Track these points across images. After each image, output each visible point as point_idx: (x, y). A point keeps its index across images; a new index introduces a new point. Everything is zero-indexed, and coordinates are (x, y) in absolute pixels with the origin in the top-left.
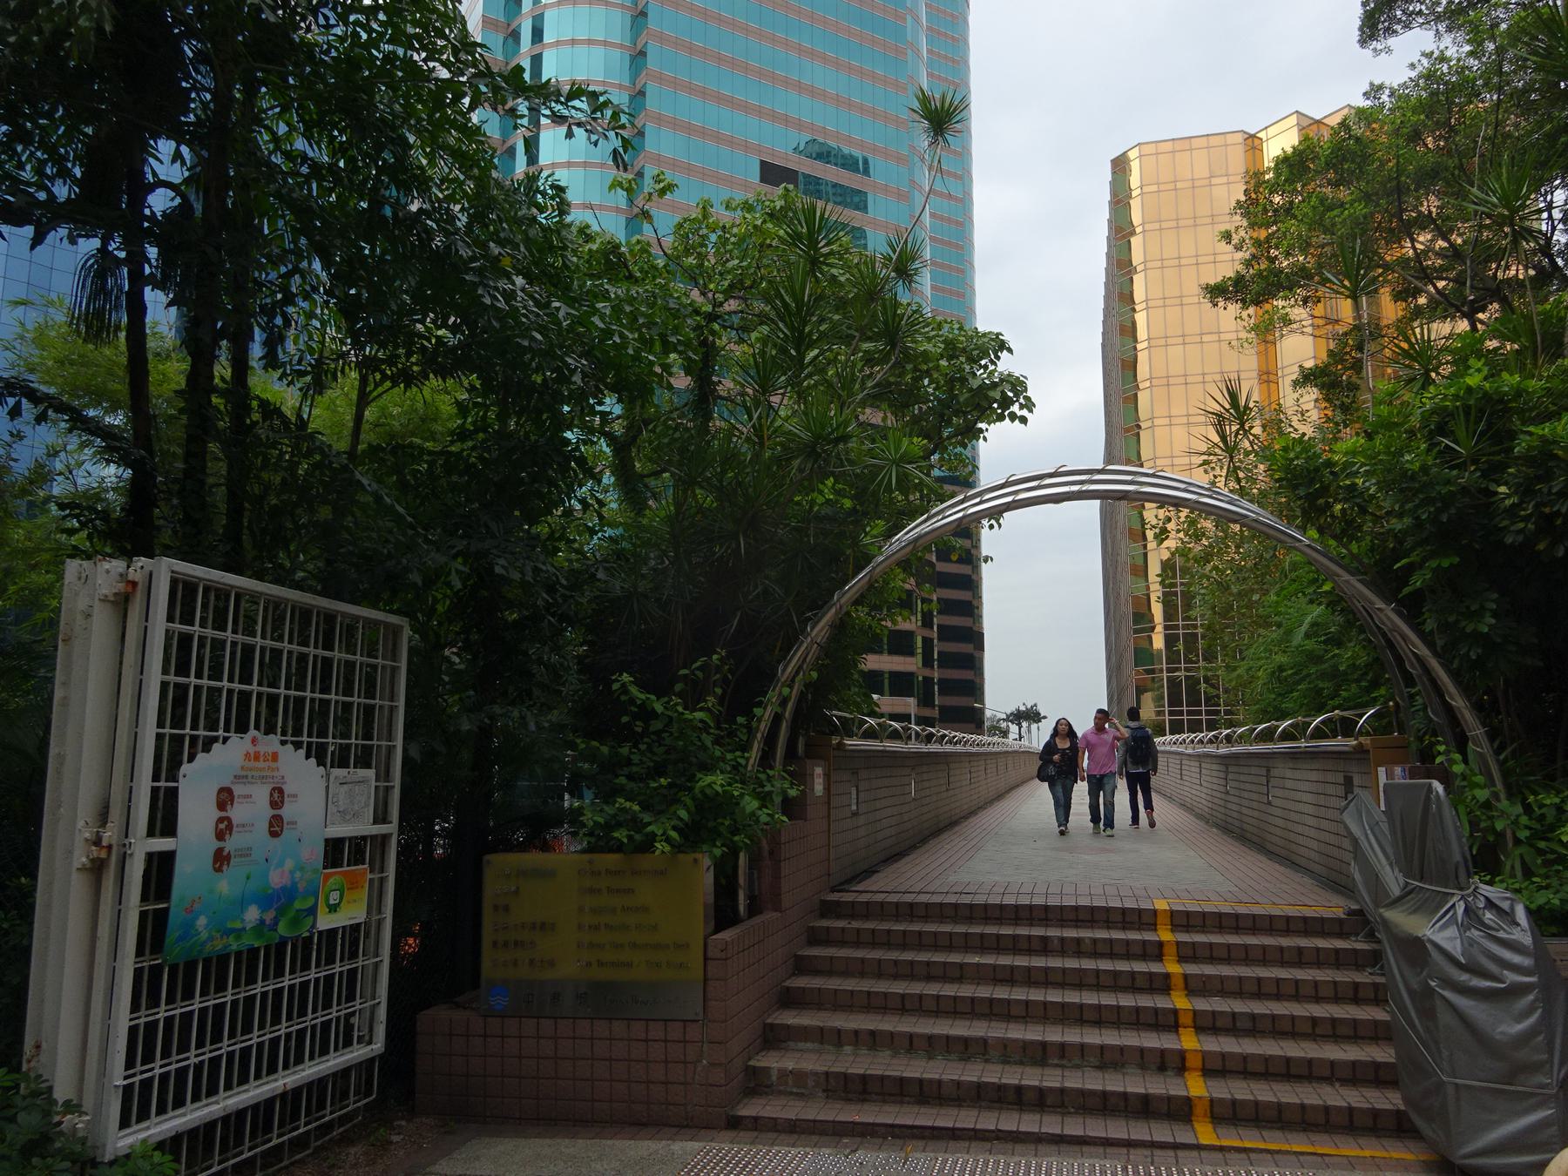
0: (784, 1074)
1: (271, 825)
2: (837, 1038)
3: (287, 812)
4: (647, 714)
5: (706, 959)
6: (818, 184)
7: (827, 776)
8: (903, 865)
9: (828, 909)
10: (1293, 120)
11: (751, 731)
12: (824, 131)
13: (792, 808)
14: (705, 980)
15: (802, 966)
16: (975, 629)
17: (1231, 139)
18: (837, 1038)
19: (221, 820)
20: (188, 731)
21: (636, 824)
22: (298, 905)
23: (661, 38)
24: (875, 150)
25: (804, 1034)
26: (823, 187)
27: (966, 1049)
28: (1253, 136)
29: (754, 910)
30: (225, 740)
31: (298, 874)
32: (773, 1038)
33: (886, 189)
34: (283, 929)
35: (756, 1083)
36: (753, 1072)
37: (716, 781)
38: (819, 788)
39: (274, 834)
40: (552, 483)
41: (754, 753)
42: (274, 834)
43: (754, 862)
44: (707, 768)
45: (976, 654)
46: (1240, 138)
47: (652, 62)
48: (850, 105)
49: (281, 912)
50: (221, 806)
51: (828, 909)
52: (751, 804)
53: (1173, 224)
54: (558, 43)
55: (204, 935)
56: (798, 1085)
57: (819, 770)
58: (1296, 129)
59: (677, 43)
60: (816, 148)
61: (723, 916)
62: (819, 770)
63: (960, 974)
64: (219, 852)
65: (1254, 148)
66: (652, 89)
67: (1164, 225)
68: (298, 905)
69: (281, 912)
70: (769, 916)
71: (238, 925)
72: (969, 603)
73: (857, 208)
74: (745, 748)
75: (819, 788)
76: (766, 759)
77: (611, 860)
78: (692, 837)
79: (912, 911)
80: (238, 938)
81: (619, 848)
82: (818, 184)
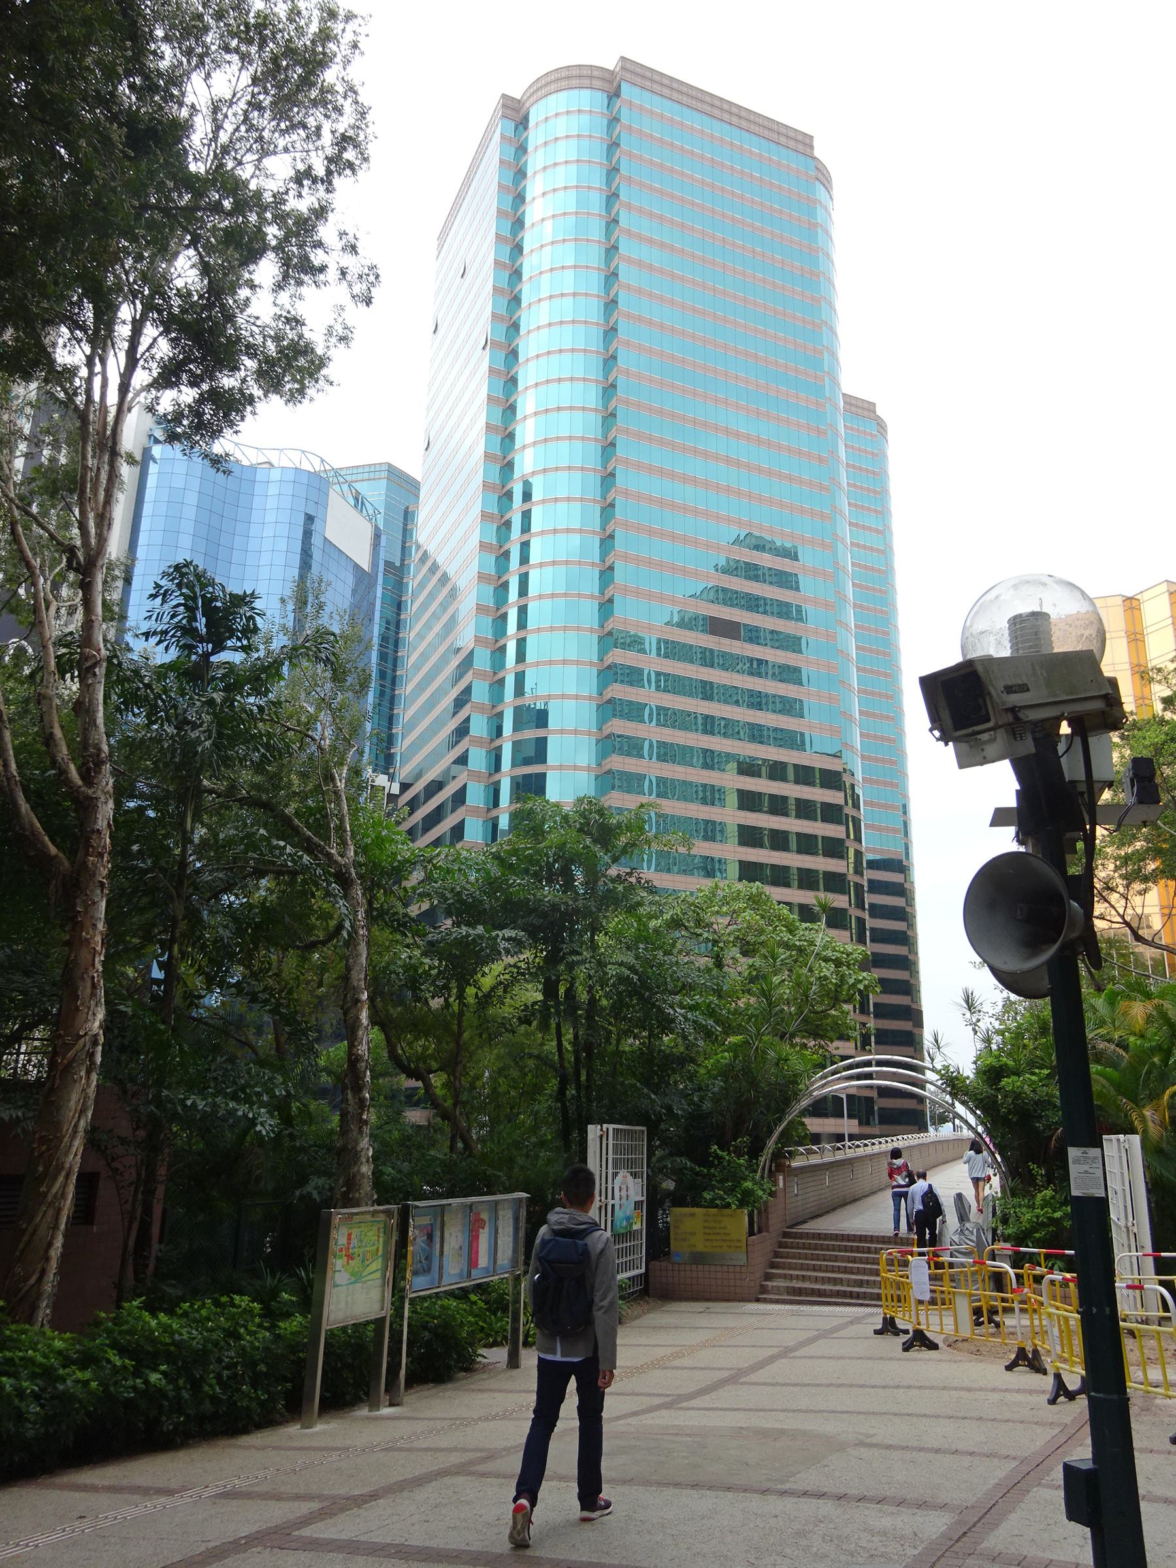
0: (773, 1287)
2: (791, 1277)
4: (720, 1158)
6: (757, 569)
7: (784, 1179)
8: (820, 1220)
9: (785, 1235)
10: (1164, 587)
11: (758, 1166)
12: (761, 528)
13: (772, 1194)
15: (776, 1255)
16: (914, 1006)
17: (1110, 601)
18: (791, 1277)
21: (723, 1199)
23: (626, 525)
24: (804, 540)
25: (779, 1276)
26: (760, 572)
27: (835, 1281)
28: (1131, 598)
29: (760, 1231)
32: (768, 1277)
33: (815, 572)
35: (764, 1289)
36: (762, 1286)
37: (748, 1184)
38: (781, 1184)
40: (41, 288)
41: (759, 1174)
43: (759, 1213)
44: (745, 1180)
45: (916, 1031)
46: (1119, 600)
47: (619, 544)
48: (779, 447)
51: (785, 1235)
52: (760, 1193)
54: (543, 533)
56: (778, 1290)
58: (1166, 595)
59: (639, 528)
60: (754, 542)
61: (751, 1233)
63: (836, 1259)
65: (1132, 608)
66: (619, 566)
70: (764, 1234)
72: (906, 982)
74: (756, 1171)
75: (781, 1184)
76: (762, 1177)
77: (714, 1210)
78: (742, 1204)
79: (819, 1236)
81: (716, 1206)
82: (757, 569)
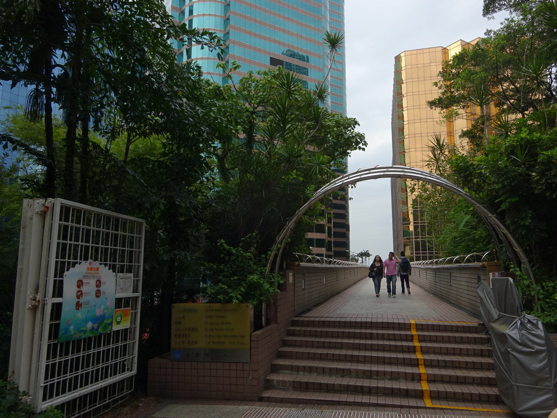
0: (278, 382)
1: (96, 293)
2: (297, 369)
3: (102, 289)
4: (230, 254)
5: (251, 341)
6: (291, 65)
7: (294, 276)
8: (321, 307)
9: (294, 323)
10: (459, 43)
11: (267, 260)
12: (293, 46)
13: (281, 287)
14: (251, 348)
15: (285, 343)
16: (346, 223)
17: (437, 49)
18: (297, 369)
19: (78, 291)
20: (67, 260)
21: (226, 293)
22: (106, 322)
23: (235, 14)
24: (311, 53)
25: (286, 367)
26: (292, 67)
27: (343, 373)
28: (445, 48)
29: (268, 323)
30: (80, 263)
31: (106, 311)
32: (275, 369)
33: (315, 67)
34: (100, 330)
35: (269, 385)
36: (267, 381)
37: (254, 278)
38: (291, 280)
39: (97, 297)
40: (196, 172)
41: (268, 268)
42: (97, 297)
43: (268, 306)
44: (251, 273)
45: (347, 232)
46: (440, 49)
47: (232, 22)
48: (302, 37)
49: (100, 324)
50: (79, 286)
51: (294, 323)
52: (267, 286)
53: (417, 80)
54: (198, 15)
55: (73, 332)
56: (283, 386)
57: (291, 274)
58: (460, 46)
59: (240, 15)
60: (290, 53)
61: (257, 325)
62: (291, 274)
63: (341, 346)
64: (78, 303)
65: (445, 53)
66: (232, 32)
67: (414, 80)
68: (106, 322)
69: (100, 324)
70: (273, 326)
71: (85, 329)
72: (344, 214)
73: (304, 74)
74: (265, 266)
75: (291, 280)
76: (272, 270)
77: (217, 306)
78: (246, 297)
79: (324, 324)
80: (85, 333)
81: (220, 301)
82: (291, 65)
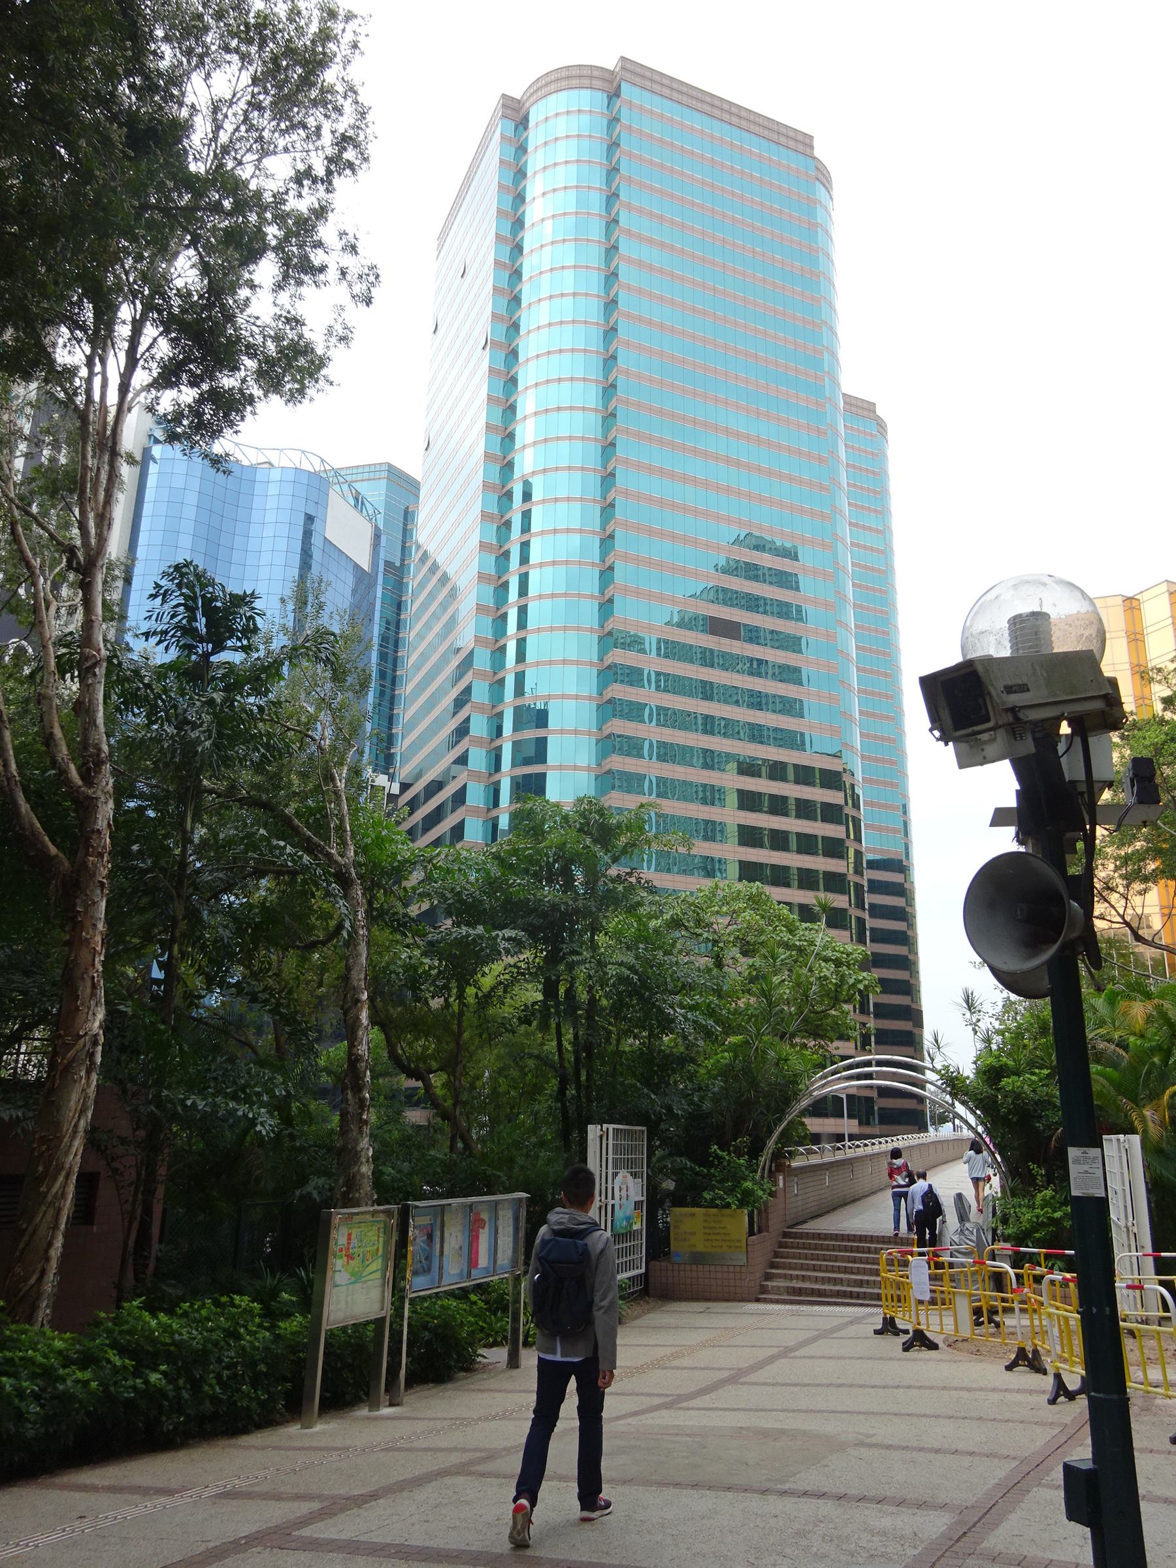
0: (773, 1287)
2: (791, 1277)
4: (720, 1158)
6: (757, 569)
7: (784, 1179)
8: (820, 1220)
9: (785, 1235)
10: (1164, 587)
11: (758, 1166)
12: (761, 528)
13: (772, 1194)
15: (776, 1255)
16: (914, 1006)
17: (1110, 601)
18: (791, 1277)
21: (723, 1199)
23: (626, 525)
24: (804, 540)
25: (779, 1276)
26: (760, 572)
27: (835, 1281)
28: (1131, 598)
29: (760, 1231)
32: (768, 1277)
33: (815, 572)
35: (764, 1289)
36: (762, 1286)
37: (748, 1184)
38: (781, 1184)
40: (41, 288)
41: (759, 1174)
43: (759, 1213)
44: (745, 1180)
45: (916, 1031)
46: (1119, 600)
47: (619, 544)
48: (779, 447)
51: (785, 1235)
52: (760, 1193)
54: (543, 533)
56: (778, 1290)
58: (1166, 595)
59: (639, 528)
60: (754, 542)
61: (751, 1233)
63: (836, 1259)
65: (1132, 608)
66: (619, 566)
70: (764, 1234)
72: (906, 982)
74: (756, 1171)
75: (781, 1184)
76: (762, 1177)
77: (714, 1210)
78: (742, 1204)
79: (819, 1236)
81: (716, 1206)
82: (757, 569)
